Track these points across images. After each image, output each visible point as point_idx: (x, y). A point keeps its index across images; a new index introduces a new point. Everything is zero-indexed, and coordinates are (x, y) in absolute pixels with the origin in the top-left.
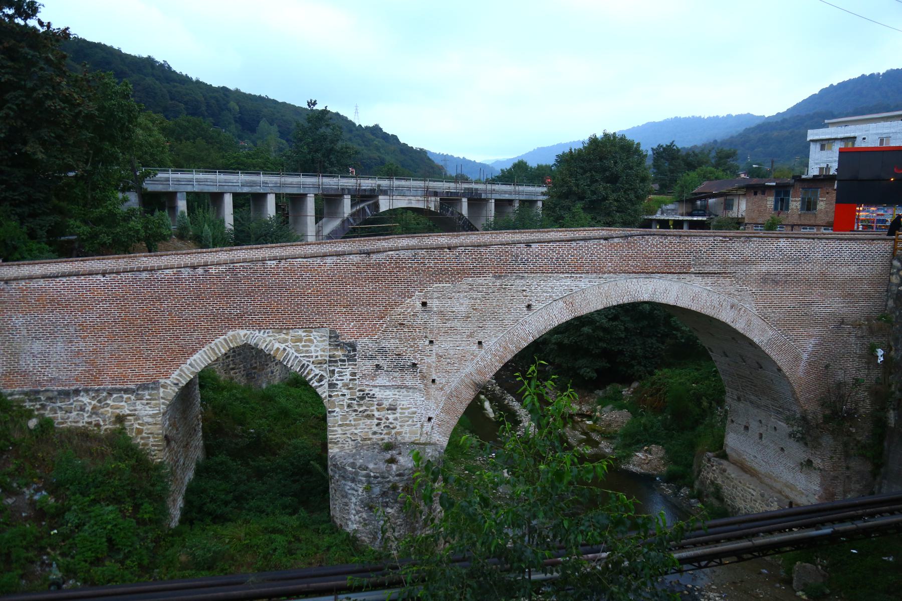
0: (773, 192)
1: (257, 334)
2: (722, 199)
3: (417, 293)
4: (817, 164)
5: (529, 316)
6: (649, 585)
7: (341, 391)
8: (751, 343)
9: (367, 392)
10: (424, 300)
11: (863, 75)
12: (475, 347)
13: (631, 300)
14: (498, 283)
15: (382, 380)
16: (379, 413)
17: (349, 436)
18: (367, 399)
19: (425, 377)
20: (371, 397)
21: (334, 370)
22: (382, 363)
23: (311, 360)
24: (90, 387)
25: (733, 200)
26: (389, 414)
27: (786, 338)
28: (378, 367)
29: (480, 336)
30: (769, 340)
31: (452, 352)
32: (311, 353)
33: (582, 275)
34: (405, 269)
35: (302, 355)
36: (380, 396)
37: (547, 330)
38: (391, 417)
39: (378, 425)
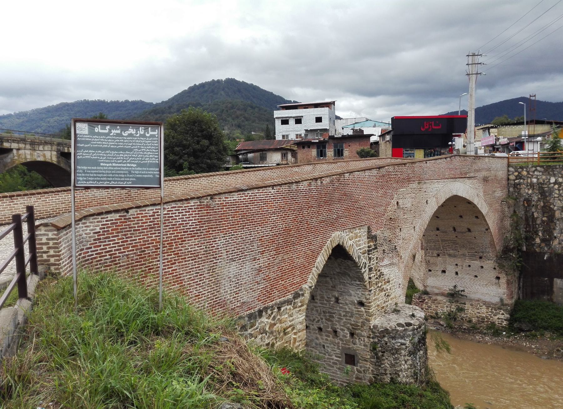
0: (315, 146)
2: (258, 154)
3: (395, 196)
4: (280, 133)
11: (213, 80)
24: (266, 305)
25: (266, 154)
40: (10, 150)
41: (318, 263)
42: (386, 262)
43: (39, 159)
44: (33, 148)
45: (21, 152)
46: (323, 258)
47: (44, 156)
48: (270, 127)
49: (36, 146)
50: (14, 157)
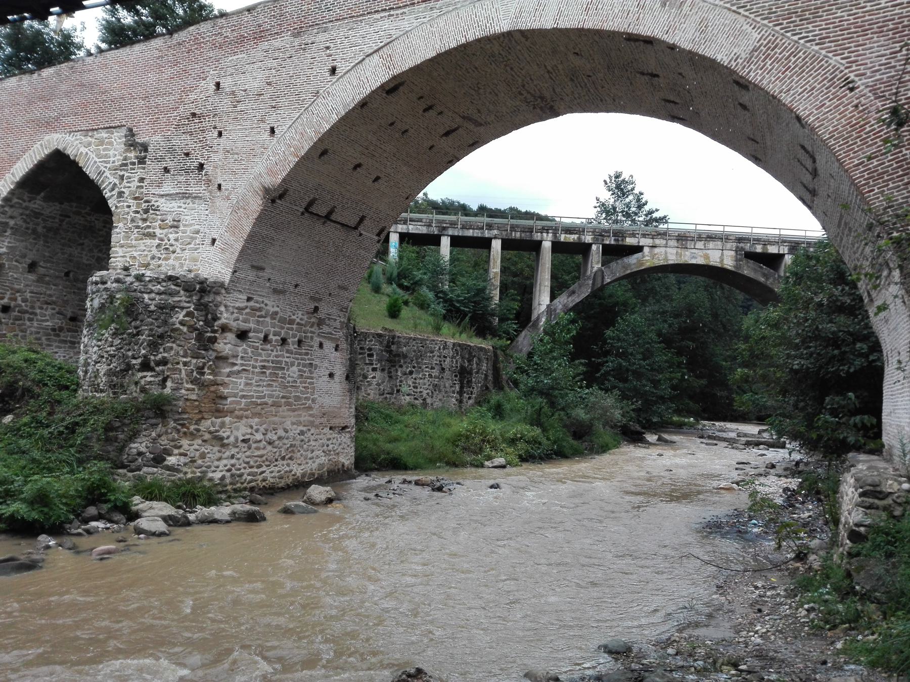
1: (67, 138)
3: (212, 72)
5: (332, 85)
6: (116, 477)
7: (127, 202)
8: (709, 65)
9: (153, 203)
10: (218, 80)
12: (266, 135)
13: (479, 34)
14: (297, 42)
15: (168, 188)
16: (161, 231)
17: (128, 260)
18: (151, 212)
19: (210, 181)
20: (154, 210)
21: (123, 175)
22: (170, 164)
23: (108, 166)
26: (171, 233)
27: (796, 38)
28: (166, 170)
29: (271, 121)
30: (754, 50)
31: (240, 144)
32: (110, 157)
33: (404, 10)
34: (202, 45)
35: (101, 160)
36: (165, 209)
37: (356, 102)
38: (172, 236)
39: (159, 246)
40: (638, 249)
41: (16, 169)
42: (168, 188)
43: (694, 261)
44: (682, 245)
45: (656, 250)
46: (25, 165)
47: (707, 257)
48: (735, 76)
49: (689, 242)
50: (644, 257)
